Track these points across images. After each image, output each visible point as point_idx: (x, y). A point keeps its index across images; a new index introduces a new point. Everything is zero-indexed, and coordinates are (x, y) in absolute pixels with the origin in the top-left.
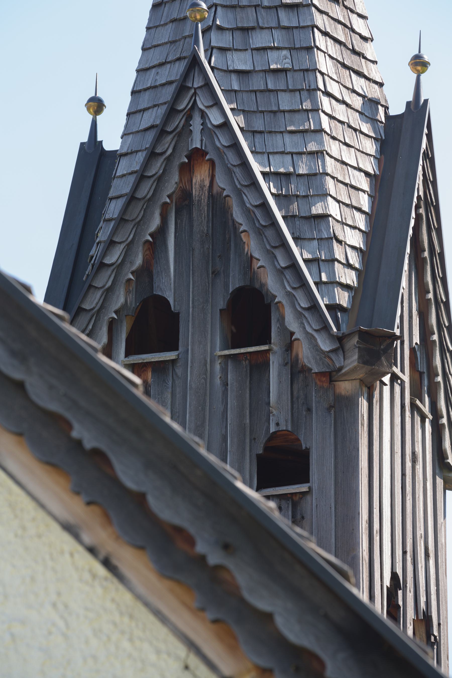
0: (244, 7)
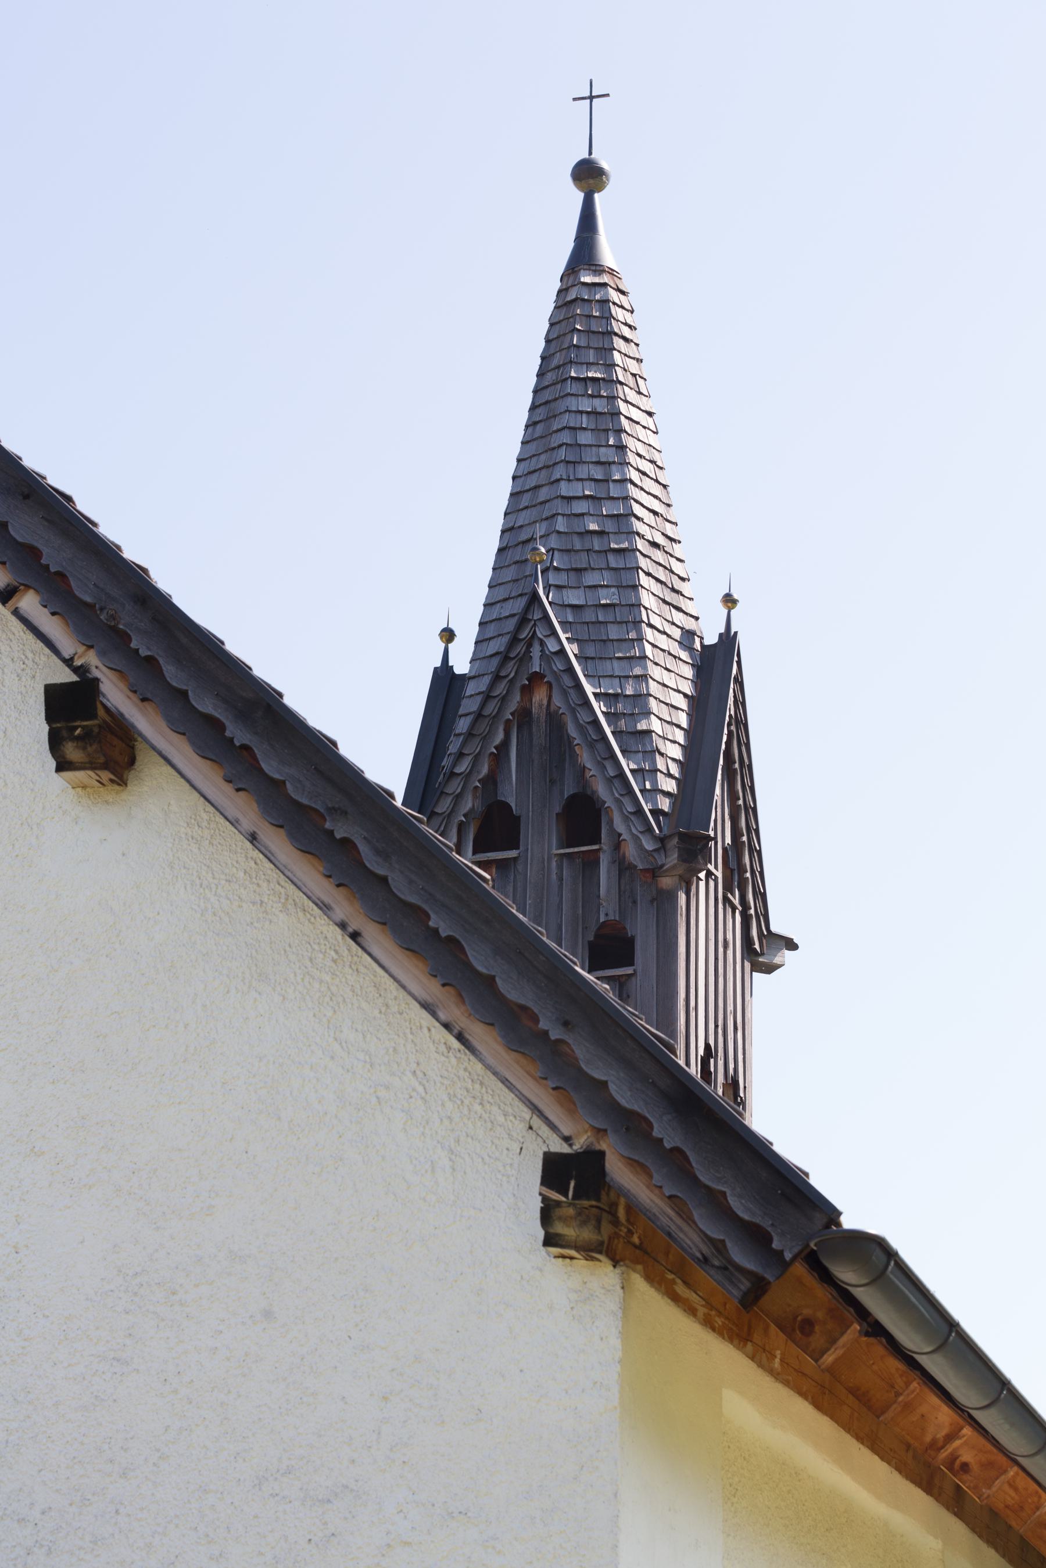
0: (578, 551)
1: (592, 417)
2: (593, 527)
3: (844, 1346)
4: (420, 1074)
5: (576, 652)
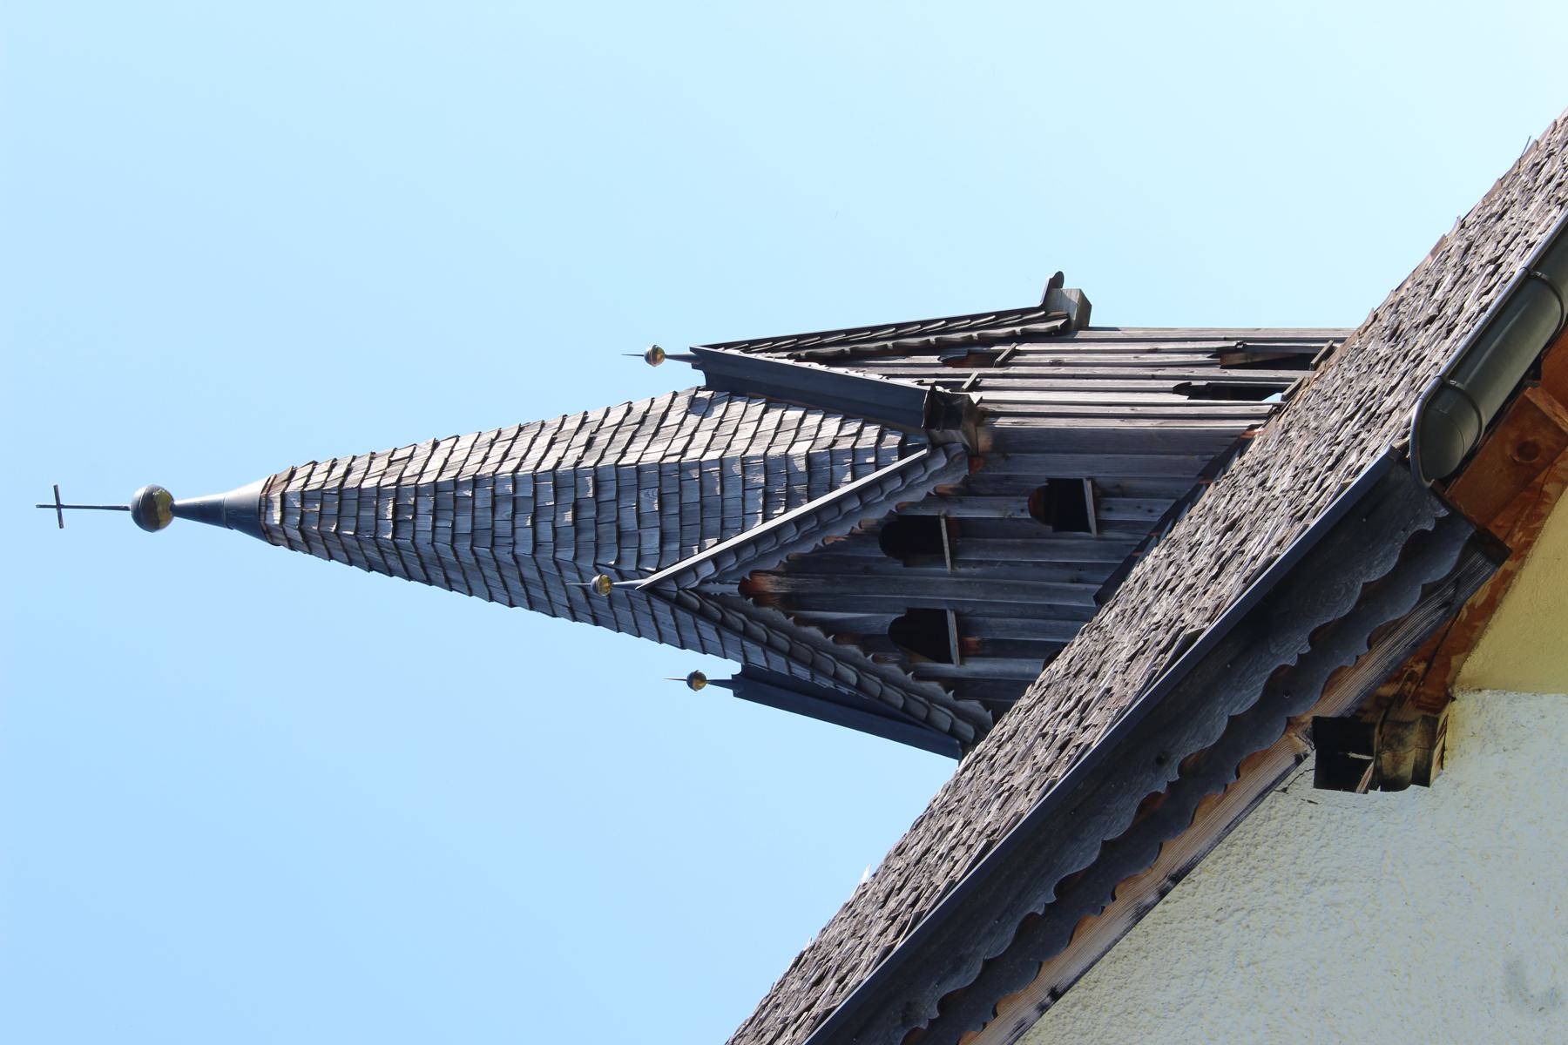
0: (597, 535)
1: (439, 515)
2: (568, 517)
3: (1552, 405)
4: (1221, 915)
5: (715, 541)
